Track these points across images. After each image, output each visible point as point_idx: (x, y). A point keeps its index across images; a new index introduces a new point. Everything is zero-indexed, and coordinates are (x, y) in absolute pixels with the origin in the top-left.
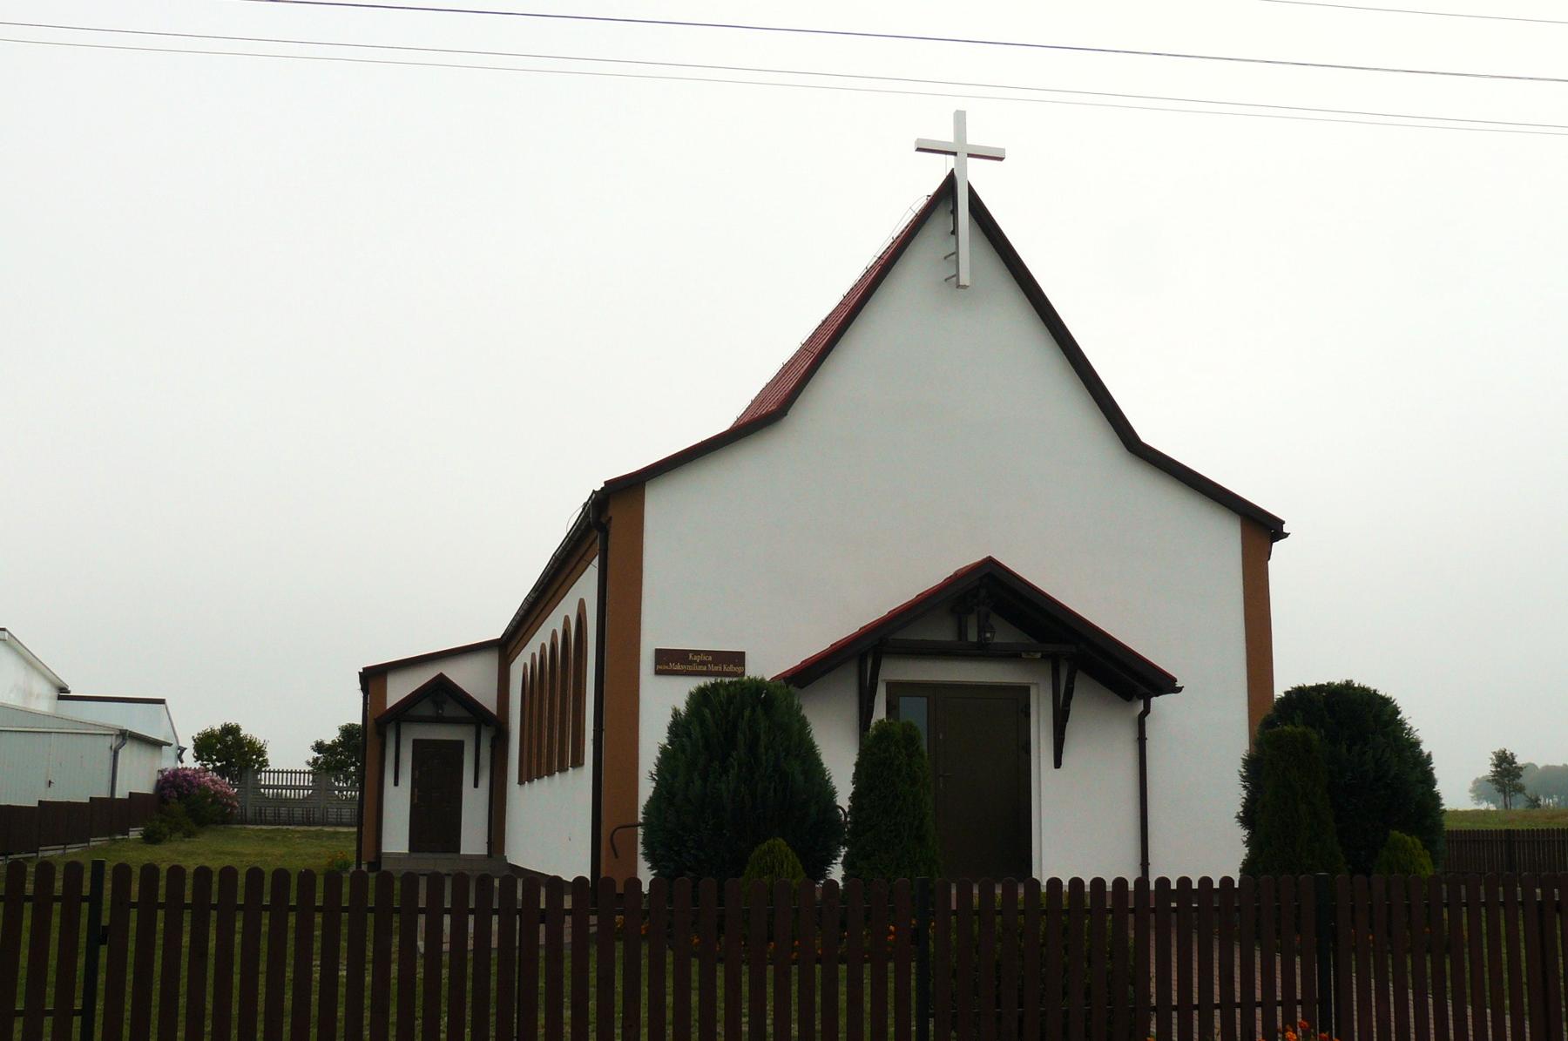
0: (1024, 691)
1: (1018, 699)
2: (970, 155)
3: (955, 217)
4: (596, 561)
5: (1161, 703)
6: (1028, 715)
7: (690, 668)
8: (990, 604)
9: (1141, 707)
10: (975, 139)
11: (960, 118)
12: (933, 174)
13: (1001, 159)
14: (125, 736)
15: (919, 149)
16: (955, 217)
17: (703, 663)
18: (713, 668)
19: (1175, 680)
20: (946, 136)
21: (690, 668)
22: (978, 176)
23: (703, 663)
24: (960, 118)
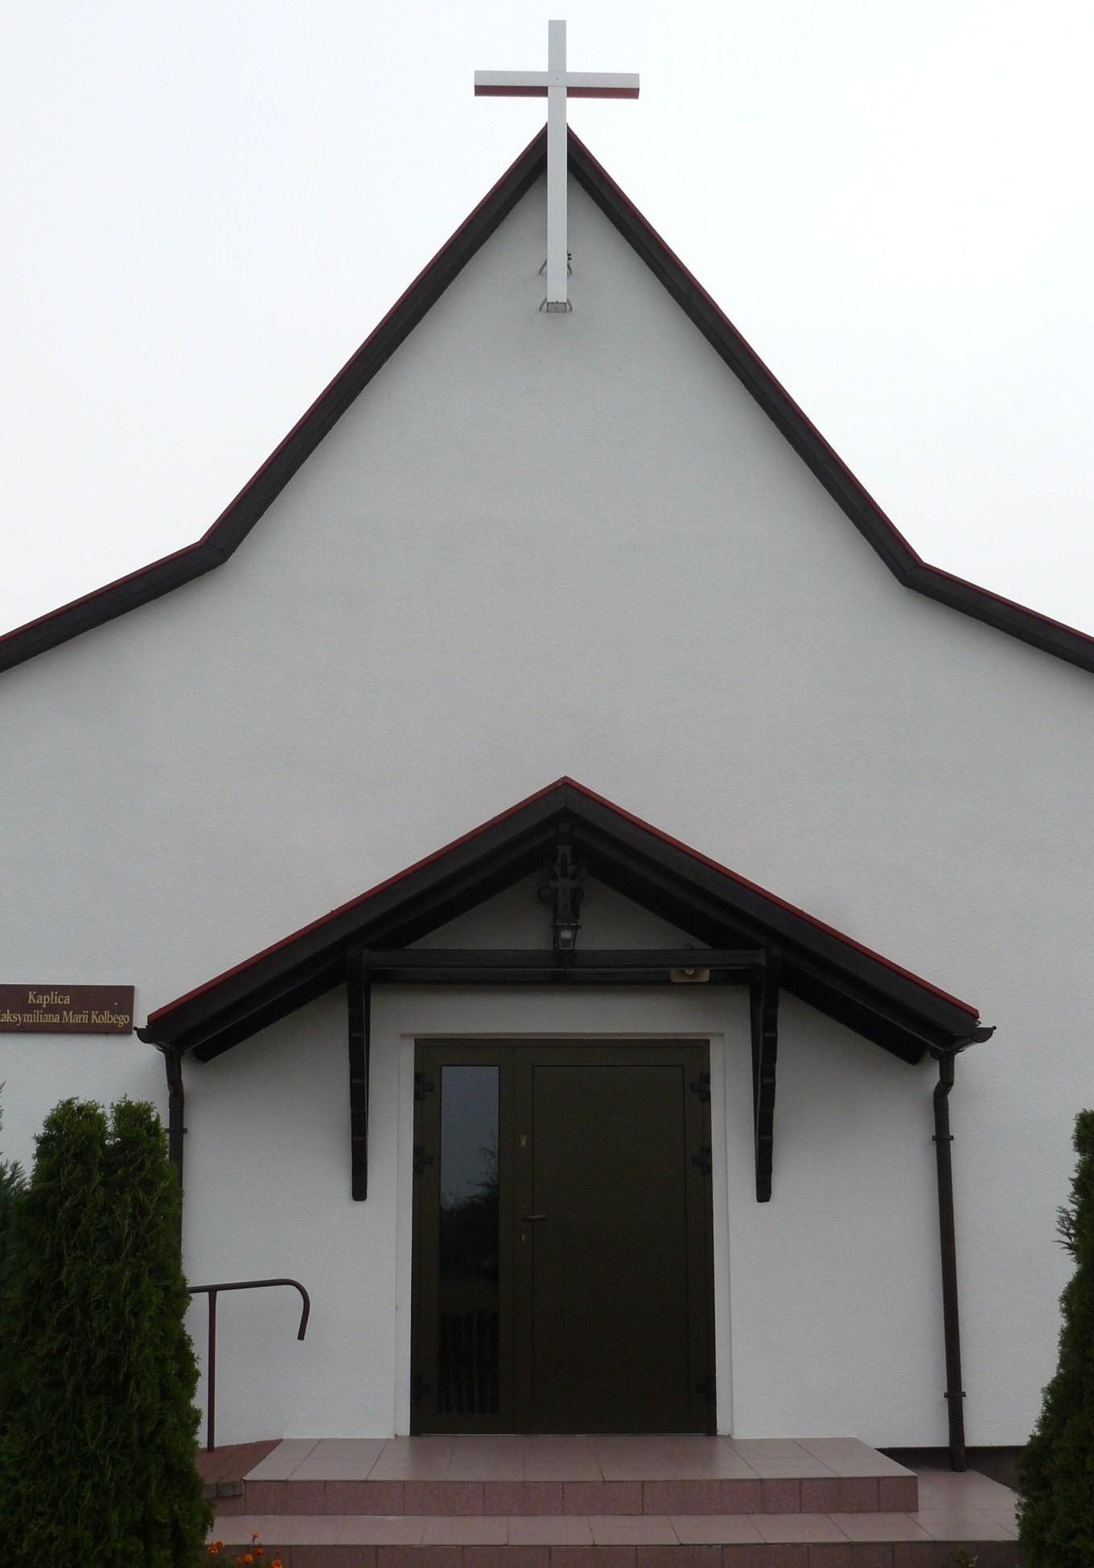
0: (698, 1049)
1: (687, 1064)
2: (574, 92)
3: (550, 201)
4: (419, 945)
5: (969, 1059)
6: (706, 1097)
7: (29, 1018)
8: (565, 870)
9: (934, 1077)
10: (582, 62)
11: (557, 31)
12: (516, 125)
13: (632, 93)
14: (643, 1482)
15: (481, 90)
16: (550, 201)
17: (52, 1009)
18: (70, 1018)
19: (973, 1015)
20: (533, 62)
21: (29, 1018)
22: (599, 127)
23: (52, 1009)
24: (557, 31)
